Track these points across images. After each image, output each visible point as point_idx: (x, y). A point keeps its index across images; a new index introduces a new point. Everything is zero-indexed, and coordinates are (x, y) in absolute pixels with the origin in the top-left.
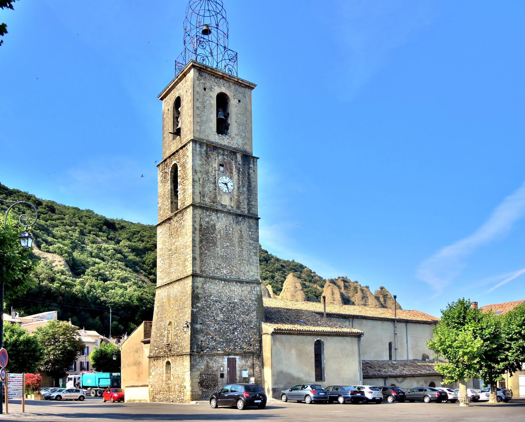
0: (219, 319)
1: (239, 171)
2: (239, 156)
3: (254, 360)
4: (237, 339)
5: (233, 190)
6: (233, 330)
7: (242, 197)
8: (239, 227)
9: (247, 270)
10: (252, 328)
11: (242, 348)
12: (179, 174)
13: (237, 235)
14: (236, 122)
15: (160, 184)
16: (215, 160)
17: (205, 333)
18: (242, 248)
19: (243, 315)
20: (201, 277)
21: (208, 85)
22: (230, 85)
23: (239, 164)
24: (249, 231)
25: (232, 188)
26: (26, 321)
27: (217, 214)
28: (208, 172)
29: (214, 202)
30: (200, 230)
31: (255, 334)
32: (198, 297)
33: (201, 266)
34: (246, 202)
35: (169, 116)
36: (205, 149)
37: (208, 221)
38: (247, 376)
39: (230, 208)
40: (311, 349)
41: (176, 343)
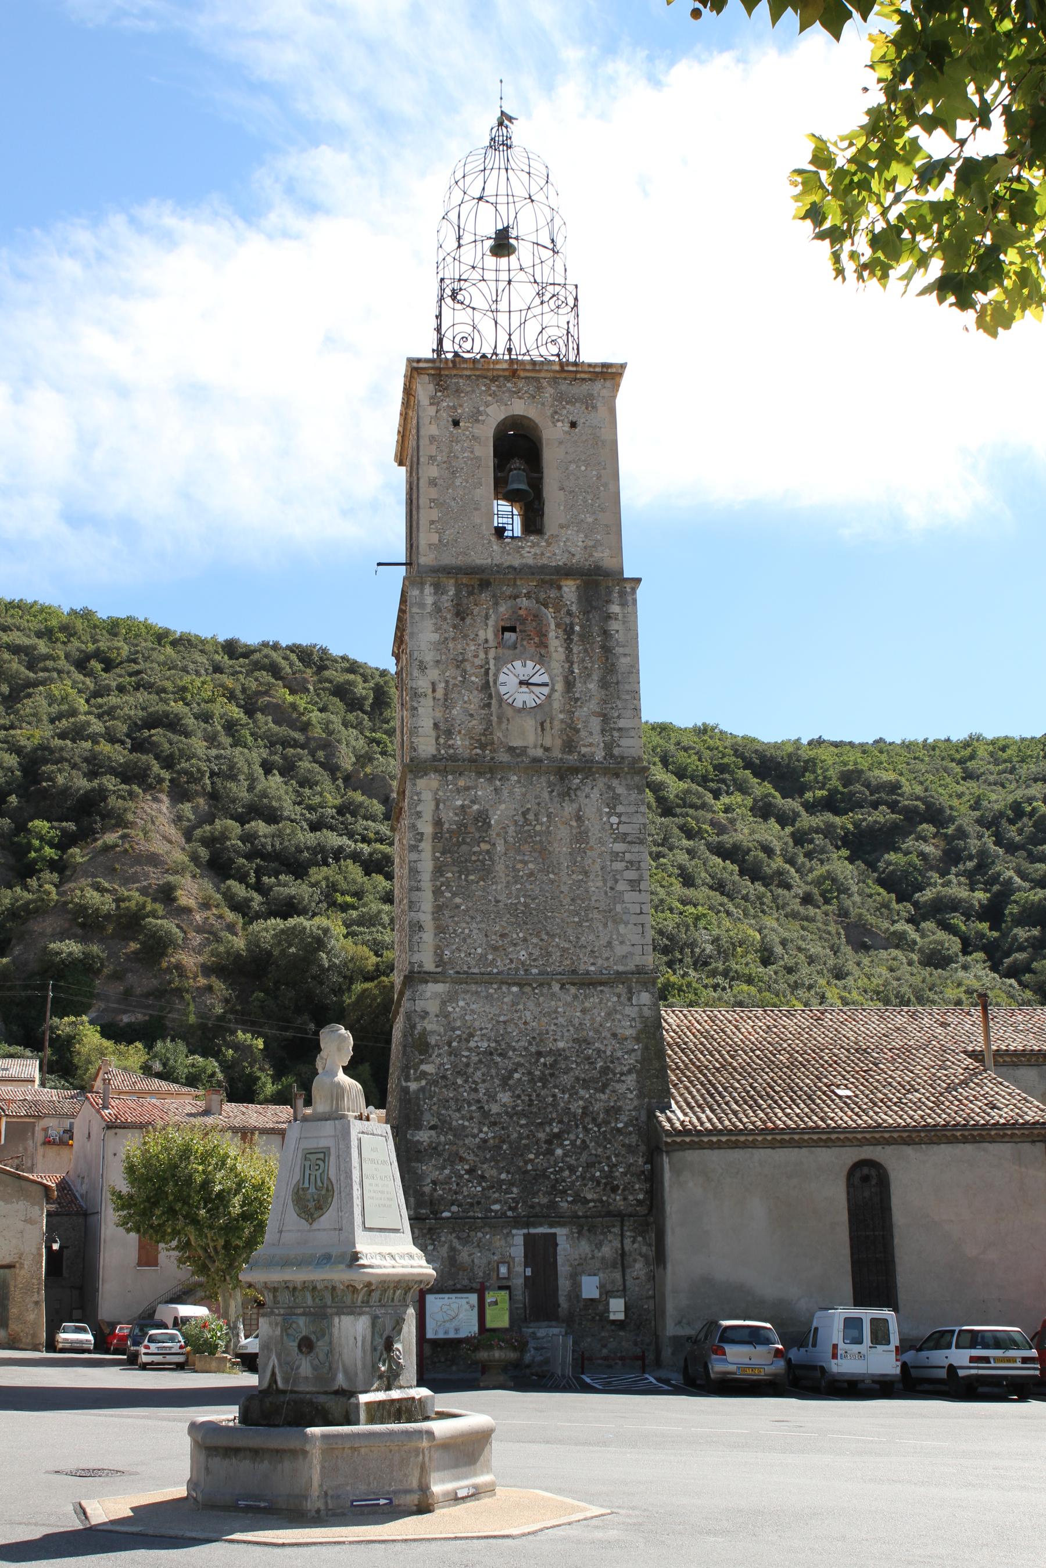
0: (495, 1108)
1: (569, 632)
2: (570, 589)
3: (627, 1241)
4: (562, 1170)
6: (549, 1142)
7: (582, 712)
8: (569, 809)
9: (603, 942)
10: (619, 1130)
11: (580, 1200)
13: (563, 833)
14: (562, 489)
15: (525, 1231)
16: (487, 617)
17: (446, 1155)
18: (586, 873)
19: (587, 1088)
21: (465, 409)
23: (569, 613)
24: (609, 815)
26: (159, 1338)
28: (464, 661)
29: (483, 747)
30: (436, 837)
33: (438, 947)
34: (595, 723)
37: (463, 806)
38: (595, 1294)
39: (539, 753)
40: (833, 1197)
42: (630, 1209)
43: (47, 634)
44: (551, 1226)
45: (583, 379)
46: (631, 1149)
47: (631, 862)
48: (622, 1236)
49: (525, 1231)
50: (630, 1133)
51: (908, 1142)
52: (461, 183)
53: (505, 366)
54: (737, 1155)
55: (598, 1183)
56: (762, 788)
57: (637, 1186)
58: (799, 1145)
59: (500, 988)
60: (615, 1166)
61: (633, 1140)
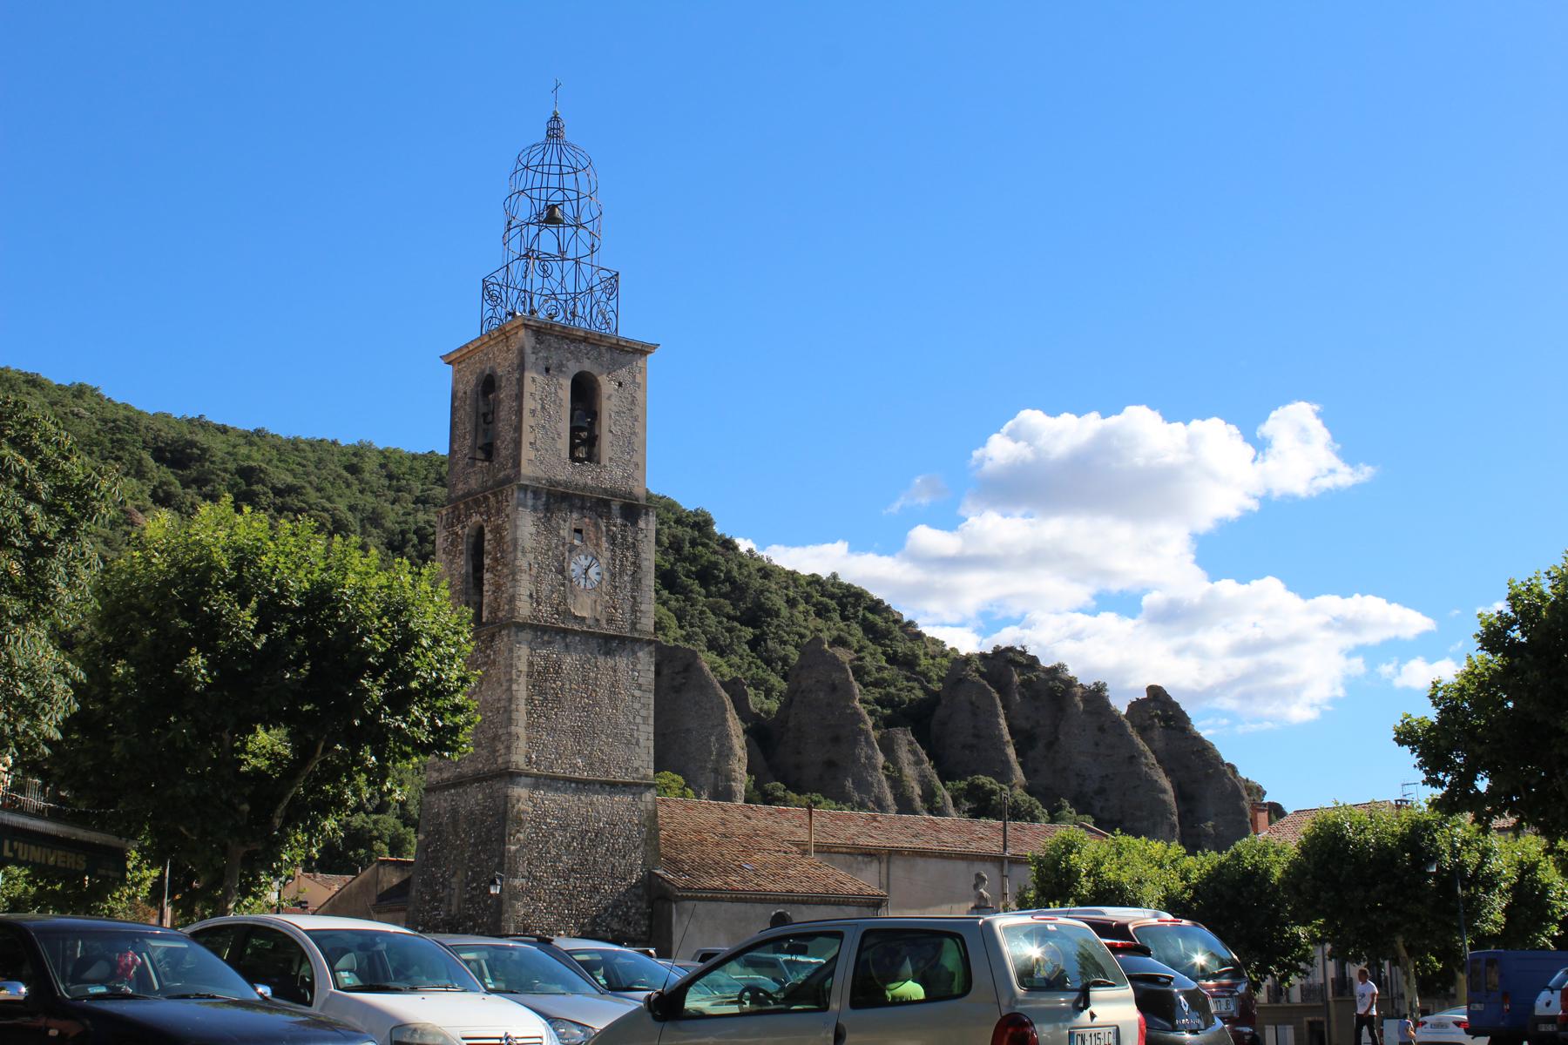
8: (611, 662)
12: (487, 547)
20: (527, 775)
21: (554, 361)
22: (600, 354)
27: (564, 638)
30: (530, 675)
41: (470, 918)
43: (355, 454)
46: (640, 898)
51: (804, 903)
54: (713, 905)
56: (160, 473)
58: (745, 901)
61: (640, 891)
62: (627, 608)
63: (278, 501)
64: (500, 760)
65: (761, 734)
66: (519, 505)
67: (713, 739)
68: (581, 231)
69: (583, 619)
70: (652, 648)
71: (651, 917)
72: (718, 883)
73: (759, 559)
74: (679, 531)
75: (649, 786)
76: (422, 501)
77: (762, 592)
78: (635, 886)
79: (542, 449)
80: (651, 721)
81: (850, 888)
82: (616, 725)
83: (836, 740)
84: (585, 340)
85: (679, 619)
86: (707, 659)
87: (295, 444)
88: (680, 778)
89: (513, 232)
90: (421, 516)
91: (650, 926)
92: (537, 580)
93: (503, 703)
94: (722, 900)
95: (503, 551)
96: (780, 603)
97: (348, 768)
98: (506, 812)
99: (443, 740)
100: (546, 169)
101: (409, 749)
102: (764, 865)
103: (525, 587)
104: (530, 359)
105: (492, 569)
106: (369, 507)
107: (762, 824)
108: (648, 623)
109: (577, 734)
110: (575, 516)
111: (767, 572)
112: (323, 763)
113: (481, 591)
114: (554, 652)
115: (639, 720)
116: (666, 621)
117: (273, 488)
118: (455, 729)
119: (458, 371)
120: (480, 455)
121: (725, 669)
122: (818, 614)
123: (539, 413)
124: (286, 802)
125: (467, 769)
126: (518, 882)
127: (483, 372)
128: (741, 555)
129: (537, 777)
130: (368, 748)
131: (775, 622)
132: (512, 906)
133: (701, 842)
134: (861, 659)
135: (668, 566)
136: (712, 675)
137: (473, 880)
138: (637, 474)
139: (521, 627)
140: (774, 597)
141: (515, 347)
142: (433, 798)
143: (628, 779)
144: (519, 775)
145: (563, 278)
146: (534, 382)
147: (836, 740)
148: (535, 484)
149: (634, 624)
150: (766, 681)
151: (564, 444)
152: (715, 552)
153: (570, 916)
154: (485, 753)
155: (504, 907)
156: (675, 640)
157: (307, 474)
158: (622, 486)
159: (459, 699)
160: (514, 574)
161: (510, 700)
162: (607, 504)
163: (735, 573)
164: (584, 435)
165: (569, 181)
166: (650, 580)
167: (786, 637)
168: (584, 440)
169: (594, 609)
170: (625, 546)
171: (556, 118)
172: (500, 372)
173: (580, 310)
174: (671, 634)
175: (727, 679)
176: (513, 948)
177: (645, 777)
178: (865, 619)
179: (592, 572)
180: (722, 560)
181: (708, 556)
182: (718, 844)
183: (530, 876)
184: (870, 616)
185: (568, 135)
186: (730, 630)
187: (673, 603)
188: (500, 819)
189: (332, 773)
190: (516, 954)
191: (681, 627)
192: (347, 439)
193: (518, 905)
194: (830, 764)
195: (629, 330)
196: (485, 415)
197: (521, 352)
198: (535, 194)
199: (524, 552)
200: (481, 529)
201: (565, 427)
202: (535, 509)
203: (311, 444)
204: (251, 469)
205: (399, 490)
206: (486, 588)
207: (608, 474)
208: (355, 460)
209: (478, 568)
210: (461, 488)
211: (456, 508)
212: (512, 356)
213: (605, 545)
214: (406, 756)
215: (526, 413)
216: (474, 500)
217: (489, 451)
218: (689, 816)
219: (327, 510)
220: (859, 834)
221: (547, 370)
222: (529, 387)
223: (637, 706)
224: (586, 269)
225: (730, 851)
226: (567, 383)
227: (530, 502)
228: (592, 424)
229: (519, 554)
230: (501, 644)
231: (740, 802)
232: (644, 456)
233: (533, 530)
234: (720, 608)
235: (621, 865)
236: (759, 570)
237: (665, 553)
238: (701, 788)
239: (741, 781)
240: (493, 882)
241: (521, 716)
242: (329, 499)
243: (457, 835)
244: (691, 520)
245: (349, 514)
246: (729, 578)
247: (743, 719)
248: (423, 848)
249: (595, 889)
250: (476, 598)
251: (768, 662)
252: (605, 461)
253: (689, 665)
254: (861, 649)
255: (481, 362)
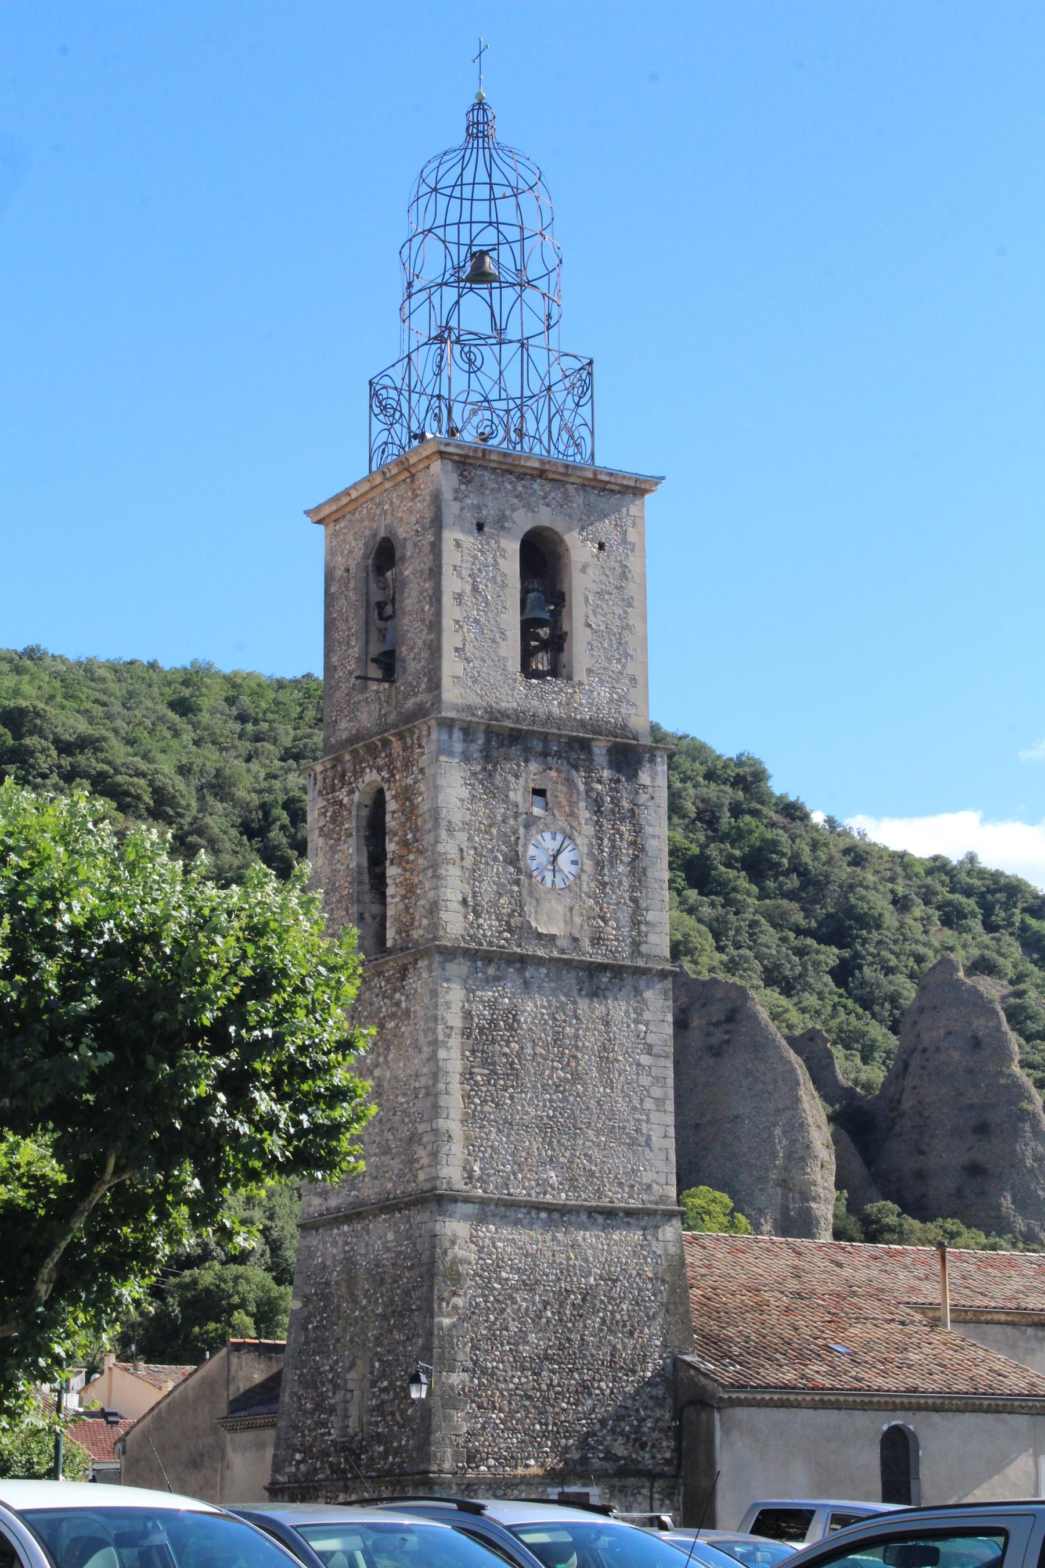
5: (578, 877)
8: (600, 1009)
11: (610, 1456)
12: (391, 823)
15: (560, 1490)
20: (467, 1200)
21: (490, 512)
24: (637, 1022)
25: (574, 869)
27: (521, 971)
30: (467, 1033)
31: (661, 1406)
32: (459, 1274)
35: (351, 594)
36: (481, 741)
41: (379, 1438)
42: (658, 1469)
43: (186, 683)
44: (584, 1485)
45: (612, 491)
46: (659, 1402)
47: (657, 1079)
48: (651, 1498)
49: (560, 1490)
50: (657, 1384)
51: (936, 1409)
52: (476, 228)
53: (536, 465)
54: (782, 1414)
55: (628, 1439)
57: (664, 1444)
58: (837, 1406)
59: (529, 1213)
60: (644, 1420)
61: (660, 1391)
62: (624, 917)
63: (66, 762)
64: (422, 1176)
65: (858, 1123)
66: (440, 752)
67: (778, 1131)
68: (529, 293)
69: (552, 938)
70: (668, 984)
71: (678, 1434)
72: (789, 1376)
73: (846, 833)
74: (711, 791)
75: (669, 1215)
76: (293, 755)
77: (851, 887)
78: (649, 1384)
79: (475, 656)
80: (670, 1106)
81: (1015, 1383)
82: (612, 1115)
83: (982, 1129)
84: (541, 474)
85: (717, 935)
86: (764, 1001)
87: (88, 669)
88: (725, 1198)
89: (416, 300)
90: (294, 780)
91: (678, 1450)
92: (473, 875)
93: (423, 1081)
94: (798, 1405)
95: (416, 830)
96: (881, 904)
97: (159, 1196)
98: (432, 1262)
99: (312, 1154)
100: (467, 192)
101: (257, 1164)
102: (868, 1345)
103: (453, 887)
104: (451, 509)
105: (400, 860)
106: (210, 768)
107: (862, 1275)
108: (659, 944)
109: (545, 1128)
110: (533, 766)
111: (858, 855)
112: (119, 1190)
113: (383, 895)
114: (505, 993)
115: (649, 1104)
116: (696, 941)
117: (57, 742)
118: (335, 1130)
119: (335, 534)
120: (374, 671)
121: (794, 1016)
122: (947, 922)
123: (468, 599)
124: (56, 1256)
125: (369, 1191)
126: (456, 1379)
127: (374, 535)
128: (815, 828)
129: (483, 1202)
130: (188, 1166)
131: (875, 936)
132: (448, 1418)
133: (760, 1307)
134: (1020, 994)
135: (695, 850)
136: (772, 1026)
137: (383, 1375)
138: (634, 695)
139: (450, 954)
140: (871, 895)
141: (426, 493)
142: (313, 1240)
143: (634, 1204)
144: (454, 1200)
145: (501, 373)
146: (458, 546)
147: (982, 1129)
148: (464, 716)
149: (636, 945)
150: (863, 1034)
151: (511, 648)
152: (773, 825)
153: (544, 1434)
154: (396, 1164)
155: (435, 1422)
156: (711, 970)
157: (109, 717)
158: (609, 715)
159: (340, 1077)
160: (434, 866)
161: (435, 1076)
162: (585, 745)
163: (806, 858)
164: (544, 632)
165: (506, 210)
166: (660, 872)
167: (893, 962)
168: (545, 640)
169: (569, 922)
170: (618, 815)
171: (480, 105)
172: (402, 532)
173: (530, 427)
174: (704, 959)
175: (798, 1032)
176: (409, 1530)
177: (663, 1199)
178: (1024, 927)
179: (565, 860)
180: (784, 837)
181: (758, 831)
182: (787, 1310)
183: (476, 1368)
184: (1033, 922)
185: (502, 132)
186: (800, 952)
187: (706, 911)
188: (424, 1274)
189: (132, 1207)
190: (412, 1540)
191: (720, 949)
192: (173, 659)
193: (458, 1416)
194: (974, 1170)
195: (613, 455)
196: (381, 606)
197: (436, 498)
198: (451, 233)
199: (450, 831)
200: (380, 794)
201: (512, 621)
202: (466, 758)
203: (116, 669)
204: (22, 712)
205: (257, 738)
206: (390, 890)
207: (584, 695)
208: (186, 692)
209: (377, 859)
210: (345, 728)
211: (338, 760)
212: (422, 507)
213: (584, 813)
214: (254, 1176)
215: (447, 600)
216: (368, 747)
217: (388, 664)
218: (739, 1262)
219: (143, 775)
220: (1027, 1291)
221: (480, 527)
222: (450, 556)
223: (645, 1081)
224: (538, 356)
225: (809, 1323)
226: (513, 547)
227: (458, 747)
228: (556, 615)
229: (443, 834)
230: (415, 983)
231: (826, 1237)
232: (645, 664)
233: (465, 793)
234: (783, 915)
235: (627, 1347)
236: (846, 852)
237: (689, 828)
238: (761, 1212)
239: (826, 1204)
240: (415, 1379)
241: (454, 1103)
242: (145, 757)
243: (354, 1299)
244: (732, 772)
245: (180, 783)
246: (797, 867)
247: (827, 1098)
248: (301, 1322)
249: (585, 1388)
250: (375, 909)
251: (866, 1003)
252: (580, 674)
253: (735, 1013)
254: (1020, 978)
255: (371, 518)
